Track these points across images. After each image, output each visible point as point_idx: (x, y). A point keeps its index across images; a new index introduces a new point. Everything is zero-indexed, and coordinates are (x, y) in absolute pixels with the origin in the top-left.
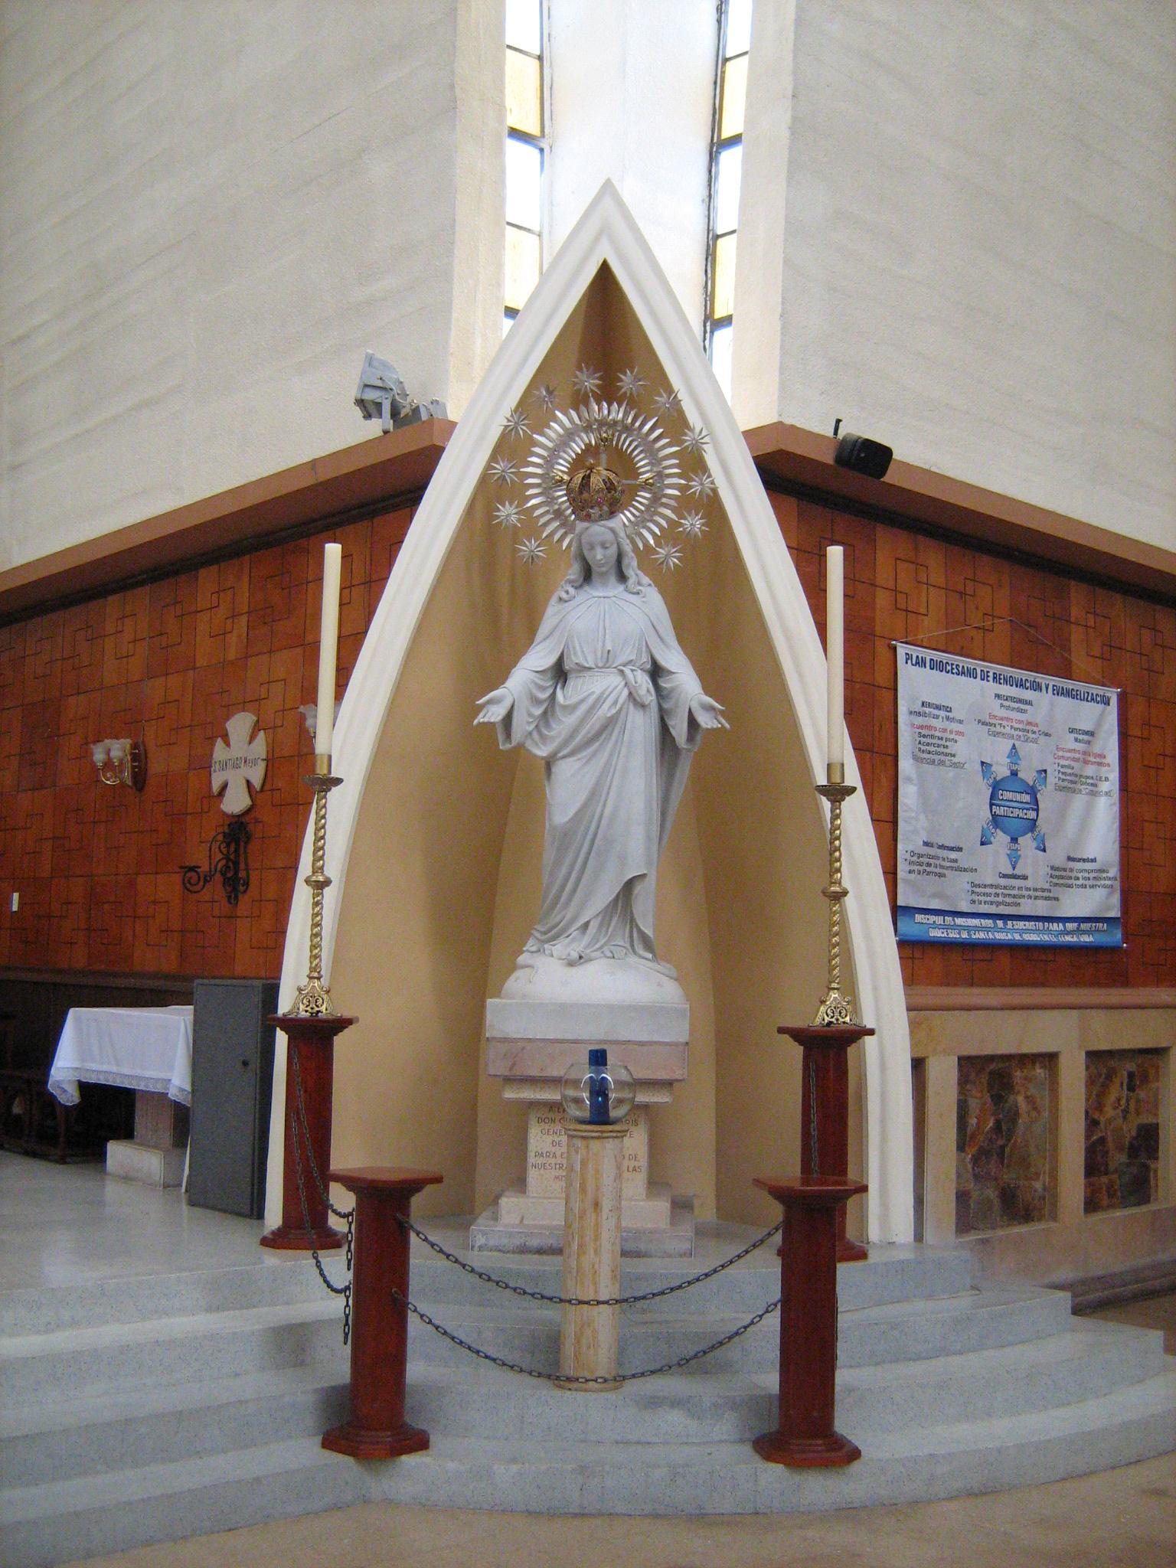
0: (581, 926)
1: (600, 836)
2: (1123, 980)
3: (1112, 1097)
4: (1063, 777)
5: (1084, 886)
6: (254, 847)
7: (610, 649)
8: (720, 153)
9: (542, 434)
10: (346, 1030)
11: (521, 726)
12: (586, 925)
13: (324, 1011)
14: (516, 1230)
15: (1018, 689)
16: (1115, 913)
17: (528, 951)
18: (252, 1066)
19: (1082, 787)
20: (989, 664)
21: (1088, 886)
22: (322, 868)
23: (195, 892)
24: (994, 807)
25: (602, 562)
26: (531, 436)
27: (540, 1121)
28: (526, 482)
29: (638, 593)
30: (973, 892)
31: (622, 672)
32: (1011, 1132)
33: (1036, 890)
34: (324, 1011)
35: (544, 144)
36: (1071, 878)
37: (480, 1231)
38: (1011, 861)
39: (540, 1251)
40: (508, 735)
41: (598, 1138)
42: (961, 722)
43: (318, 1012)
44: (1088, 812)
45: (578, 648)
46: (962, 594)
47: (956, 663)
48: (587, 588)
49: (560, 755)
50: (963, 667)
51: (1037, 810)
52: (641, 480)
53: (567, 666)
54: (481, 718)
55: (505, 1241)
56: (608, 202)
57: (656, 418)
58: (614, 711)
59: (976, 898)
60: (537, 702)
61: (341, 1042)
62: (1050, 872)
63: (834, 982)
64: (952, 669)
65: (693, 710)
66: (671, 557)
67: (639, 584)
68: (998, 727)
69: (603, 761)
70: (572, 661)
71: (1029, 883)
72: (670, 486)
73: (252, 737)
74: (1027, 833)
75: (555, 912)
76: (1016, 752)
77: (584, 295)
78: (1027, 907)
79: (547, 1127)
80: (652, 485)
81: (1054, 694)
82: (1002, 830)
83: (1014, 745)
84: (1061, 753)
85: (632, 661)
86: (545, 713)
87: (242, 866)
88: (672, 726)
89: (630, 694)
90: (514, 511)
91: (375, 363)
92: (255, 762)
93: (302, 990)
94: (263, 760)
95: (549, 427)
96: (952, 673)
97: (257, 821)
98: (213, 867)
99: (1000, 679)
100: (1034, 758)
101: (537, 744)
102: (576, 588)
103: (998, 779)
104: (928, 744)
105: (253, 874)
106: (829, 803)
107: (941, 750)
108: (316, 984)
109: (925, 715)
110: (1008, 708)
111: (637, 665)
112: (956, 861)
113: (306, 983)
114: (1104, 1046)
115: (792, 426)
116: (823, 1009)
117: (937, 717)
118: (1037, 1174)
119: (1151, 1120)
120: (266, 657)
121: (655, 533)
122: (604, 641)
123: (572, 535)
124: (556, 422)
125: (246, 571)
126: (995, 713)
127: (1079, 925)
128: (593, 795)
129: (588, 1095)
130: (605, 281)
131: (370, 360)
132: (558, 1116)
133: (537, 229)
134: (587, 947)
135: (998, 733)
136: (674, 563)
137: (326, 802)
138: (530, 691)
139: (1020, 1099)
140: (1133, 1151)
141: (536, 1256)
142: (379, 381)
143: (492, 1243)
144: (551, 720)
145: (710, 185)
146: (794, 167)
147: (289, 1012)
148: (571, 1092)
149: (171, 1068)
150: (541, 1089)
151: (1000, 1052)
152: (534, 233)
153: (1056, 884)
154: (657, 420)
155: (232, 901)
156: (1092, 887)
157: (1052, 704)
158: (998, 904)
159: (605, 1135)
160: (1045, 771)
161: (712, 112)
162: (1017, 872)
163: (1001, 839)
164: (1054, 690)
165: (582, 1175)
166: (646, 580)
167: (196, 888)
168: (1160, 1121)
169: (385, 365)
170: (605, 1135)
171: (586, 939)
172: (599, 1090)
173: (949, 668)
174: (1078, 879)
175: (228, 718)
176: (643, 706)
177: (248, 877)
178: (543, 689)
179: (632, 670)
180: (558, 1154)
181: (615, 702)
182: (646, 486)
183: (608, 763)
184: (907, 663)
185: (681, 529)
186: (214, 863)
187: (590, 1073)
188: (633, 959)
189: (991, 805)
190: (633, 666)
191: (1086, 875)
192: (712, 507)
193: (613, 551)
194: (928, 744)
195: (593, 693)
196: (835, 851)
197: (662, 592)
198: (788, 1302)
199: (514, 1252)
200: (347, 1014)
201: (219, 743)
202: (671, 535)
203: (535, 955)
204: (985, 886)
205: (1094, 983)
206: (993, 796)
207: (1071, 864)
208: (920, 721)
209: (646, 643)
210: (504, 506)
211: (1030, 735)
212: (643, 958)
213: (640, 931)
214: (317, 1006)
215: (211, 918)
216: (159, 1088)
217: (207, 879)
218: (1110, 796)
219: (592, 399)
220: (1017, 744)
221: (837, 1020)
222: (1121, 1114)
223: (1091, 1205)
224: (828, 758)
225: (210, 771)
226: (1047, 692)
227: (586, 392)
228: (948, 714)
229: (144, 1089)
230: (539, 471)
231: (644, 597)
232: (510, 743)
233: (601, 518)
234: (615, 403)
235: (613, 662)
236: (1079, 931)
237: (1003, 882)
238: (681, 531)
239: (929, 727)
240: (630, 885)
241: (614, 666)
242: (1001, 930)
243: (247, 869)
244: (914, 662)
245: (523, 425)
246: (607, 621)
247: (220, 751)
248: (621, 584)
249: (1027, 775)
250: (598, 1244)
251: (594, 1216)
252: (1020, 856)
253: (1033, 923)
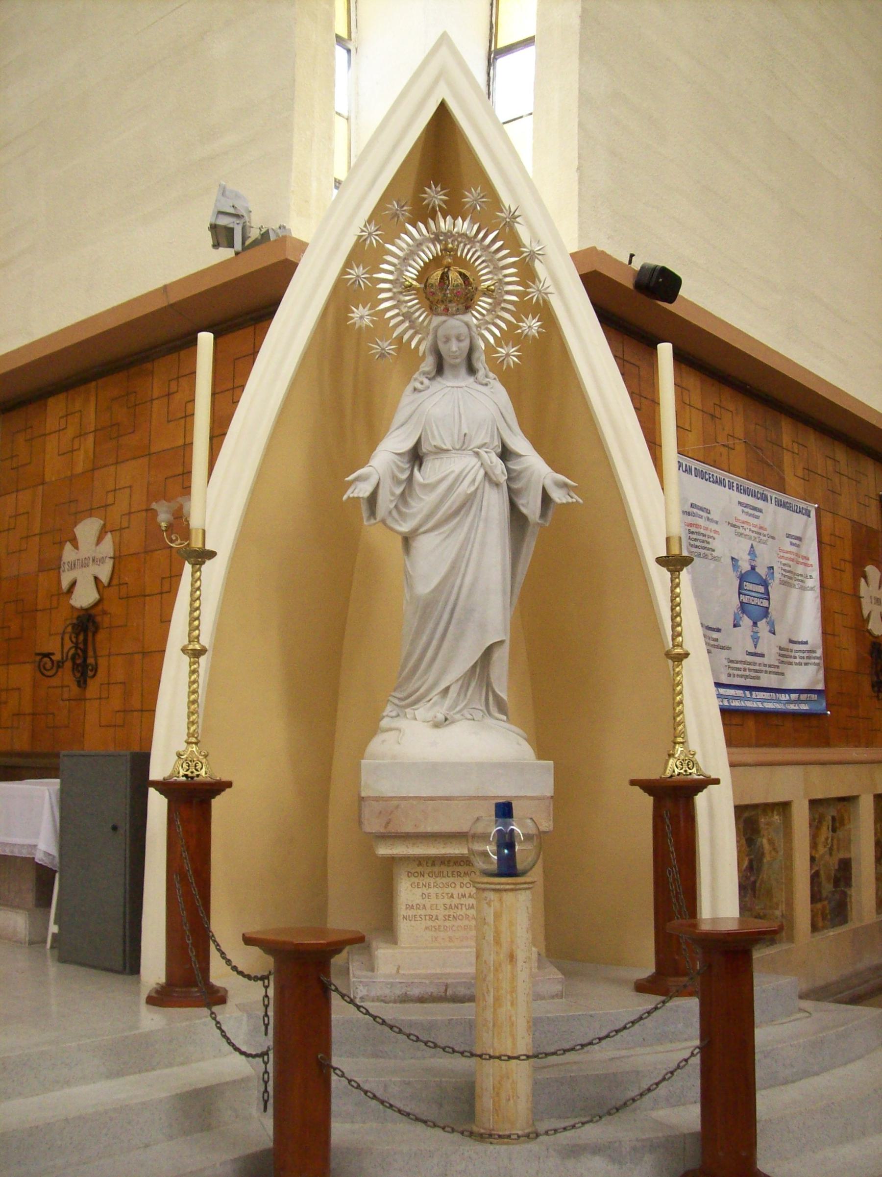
0: (441, 692)
1: (461, 603)
2: (825, 742)
3: (822, 838)
4: (784, 573)
5: (800, 664)
6: (101, 636)
8: (497, 59)
9: (393, 244)
10: (223, 793)
11: (385, 503)
12: (447, 690)
13: (203, 774)
14: (397, 981)
15: (753, 498)
16: (820, 686)
17: (387, 716)
18: (121, 831)
19: (796, 583)
20: (735, 477)
21: (803, 664)
22: (198, 637)
23: (50, 676)
24: (741, 595)
25: (457, 354)
26: (383, 246)
27: (410, 874)
28: (378, 286)
29: (486, 385)
30: (729, 667)
31: (477, 454)
32: (759, 869)
33: (770, 666)
34: (203, 774)
35: (351, 46)
36: (791, 657)
37: (361, 982)
38: (754, 642)
39: (421, 1000)
40: (373, 512)
41: (512, 890)
42: (717, 522)
43: (198, 776)
44: (800, 601)
45: (436, 433)
46: (713, 416)
47: (712, 473)
48: (439, 379)
49: (422, 530)
50: (717, 477)
51: (768, 599)
52: (483, 287)
53: (425, 448)
54: (350, 494)
55: (387, 991)
56: (444, 51)
57: (497, 231)
58: (472, 489)
59: (731, 672)
60: (398, 482)
61: (218, 804)
62: (779, 651)
63: (680, 737)
64: (710, 478)
65: (546, 487)
66: (510, 354)
67: (487, 376)
68: (741, 528)
69: (462, 536)
70: (430, 444)
71: (765, 660)
72: (508, 293)
73: (100, 540)
74: (763, 619)
75: (415, 678)
76: (754, 550)
77: (424, 130)
78: (766, 681)
79: (416, 880)
80: (493, 291)
81: (776, 505)
82: (747, 615)
83: (752, 545)
84: (782, 554)
85: (485, 444)
86: (403, 494)
87: (90, 653)
88: (523, 505)
89: (486, 474)
90: (367, 313)
91: (227, 193)
92: (102, 560)
93: (182, 755)
94: (110, 558)
95: (400, 238)
96: (710, 481)
97: (105, 613)
98: (65, 655)
99: (741, 489)
100: (766, 557)
101: (397, 521)
102: (430, 379)
103: (743, 572)
104: (695, 540)
105: (102, 662)
106: (669, 573)
107: (705, 545)
108: (194, 749)
109: (694, 515)
110: (747, 513)
111: (492, 447)
112: (717, 640)
113: (184, 748)
114: (819, 796)
115: (603, 252)
116: (672, 761)
117: (701, 517)
118: (777, 904)
119: (847, 856)
120: (112, 469)
121: (496, 335)
122: (460, 426)
123: (420, 336)
124: (406, 234)
125: (93, 399)
126: (740, 518)
127: (799, 696)
128: (454, 567)
129: (495, 848)
130: (443, 110)
131: (223, 192)
132: (466, 869)
133: (346, 114)
134: (452, 708)
135: (741, 534)
136: (514, 362)
137: (200, 575)
138: (393, 472)
139: (765, 841)
140: (836, 882)
141: (418, 1005)
142: (232, 208)
143: (373, 994)
144: (409, 500)
145: (489, 85)
146: (584, 49)
147: (170, 776)
148: (478, 847)
149: (37, 834)
150: (414, 844)
151: (832, 796)
152: (343, 117)
153: (782, 662)
154: (498, 234)
155: (82, 685)
156: (806, 664)
157: (775, 513)
158: (746, 677)
159: (518, 887)
160: (772, 568)
161: (489, 27)
162: (759, 651)
163: (746, 622)
164: (776, 501)
165: (496, 927)
166: (491, 375)
167: (48, 673)
168: (853, 856)
169: (237, 196)
170: (518, 887)
171: (448, 701)
172: (507, 841)
173: (707, 477)
174: (795, 658)
175: (75, 524)
176: (497, 485)
177: (96, 664)
178: (402, 470)
180: (428, 906)
181: (474, 481)
182: (488, 292)
183: (467, 539)
184: (679, 469)
185: (519, 331)
186: (65, 650)
187: (497, 827)
188: (489, 721)
189: (740, 593)
190: (487, 448)
191: (801, 655)
192: (544, 312)
193: (465, 344)
194: (695, 540)
195: (453, 472)
196: (676, 617)
197: (504, 384)
198: (707, 1049)
199: (395, 1002)
200: (225, 778)
201: (68, 547)
202: (510, 336)
203: (396, 719)
204: (737, 662)
205: (808, 744)
206: (740, 587)
207: (792, 646)
208: (690, 519)
210: (357, 309)
211: (762, 537)
212: (499, 720)
213: (496, 695)
214: (197, 770)
215: (61, 702)
216: (25, 854)
217: (60, 665)
218: (814, 590)
219: (439, 213)
220: (755, 544)
221: (686, 771)
222: (828, 851)
223: (815, 928)
224: (667, 532)
225: (59, 572)
226: (771, 503)
227: (434, 208)
228: (709, 515)
229: (10, 854)
230: (390, 277)
231: (492, 388)
232: (375, 519)
233: (458, 312)
234: (460, 217)
235: (469, 445)
236: (799, 701)
237: (750, 659)
238: (519, 333)
239: (697, 526)
240: (488, 652)
241: (470, 448)
242: (748, 699)
243: (96, 657)
244: (684, 469)
245: (376, 235)
246: (461, 407)
247: (69, 553)
248: (471, 376)
249: (762, 571)
250: (515, 996)
251: (509, 967)
252: (759, 637)
253: (768, 694)
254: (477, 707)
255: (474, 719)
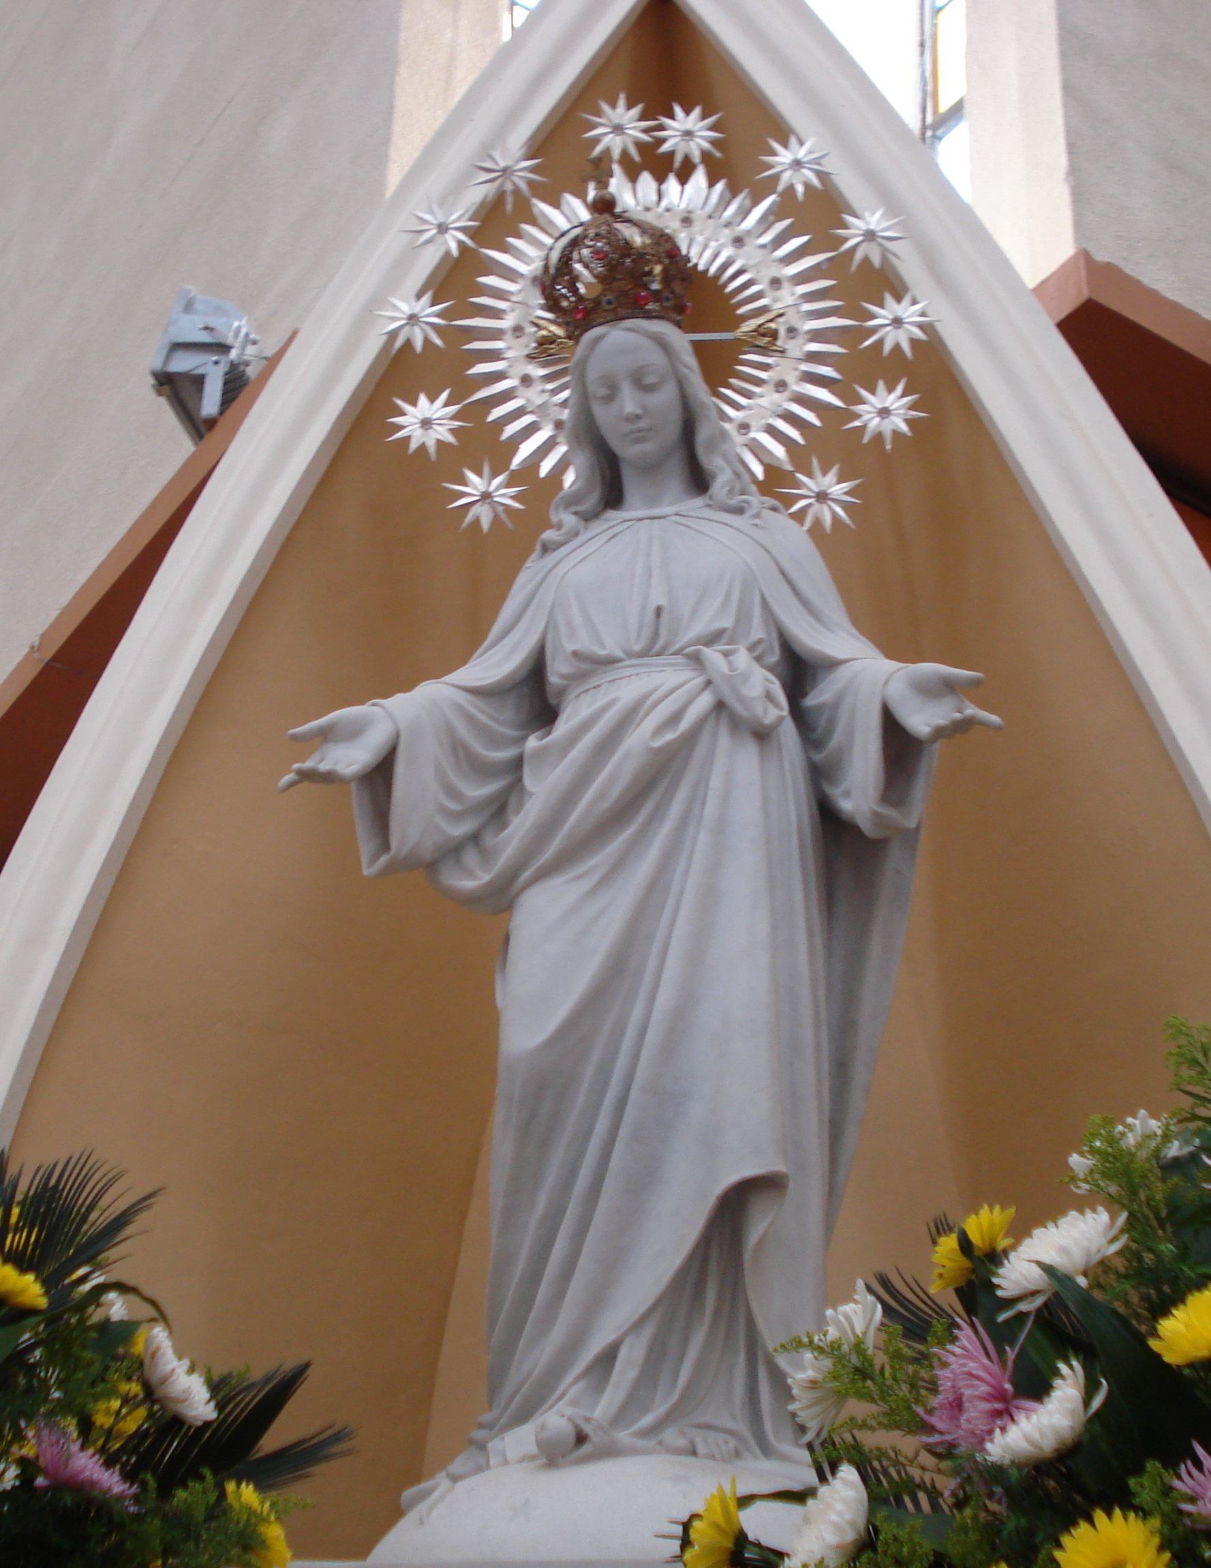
7: (662, 602)
9: (505, 249)
12: (608, 1357)
31: (697, 660)
45: (578, 619)
48: (612, 514)
53: (557, 672)
60: (480, 769)
142: (204, 333)
178: (496, 741)
179: (726, 654)
181: (675, 718)
183: (657, 885)
185: (857, 423)
193: (666, 396)
209: (765, 603)
254: (719, 1422)
255: (694, 1453)
